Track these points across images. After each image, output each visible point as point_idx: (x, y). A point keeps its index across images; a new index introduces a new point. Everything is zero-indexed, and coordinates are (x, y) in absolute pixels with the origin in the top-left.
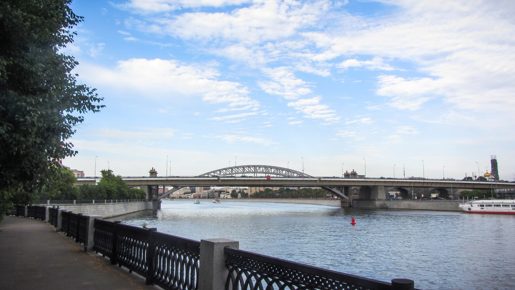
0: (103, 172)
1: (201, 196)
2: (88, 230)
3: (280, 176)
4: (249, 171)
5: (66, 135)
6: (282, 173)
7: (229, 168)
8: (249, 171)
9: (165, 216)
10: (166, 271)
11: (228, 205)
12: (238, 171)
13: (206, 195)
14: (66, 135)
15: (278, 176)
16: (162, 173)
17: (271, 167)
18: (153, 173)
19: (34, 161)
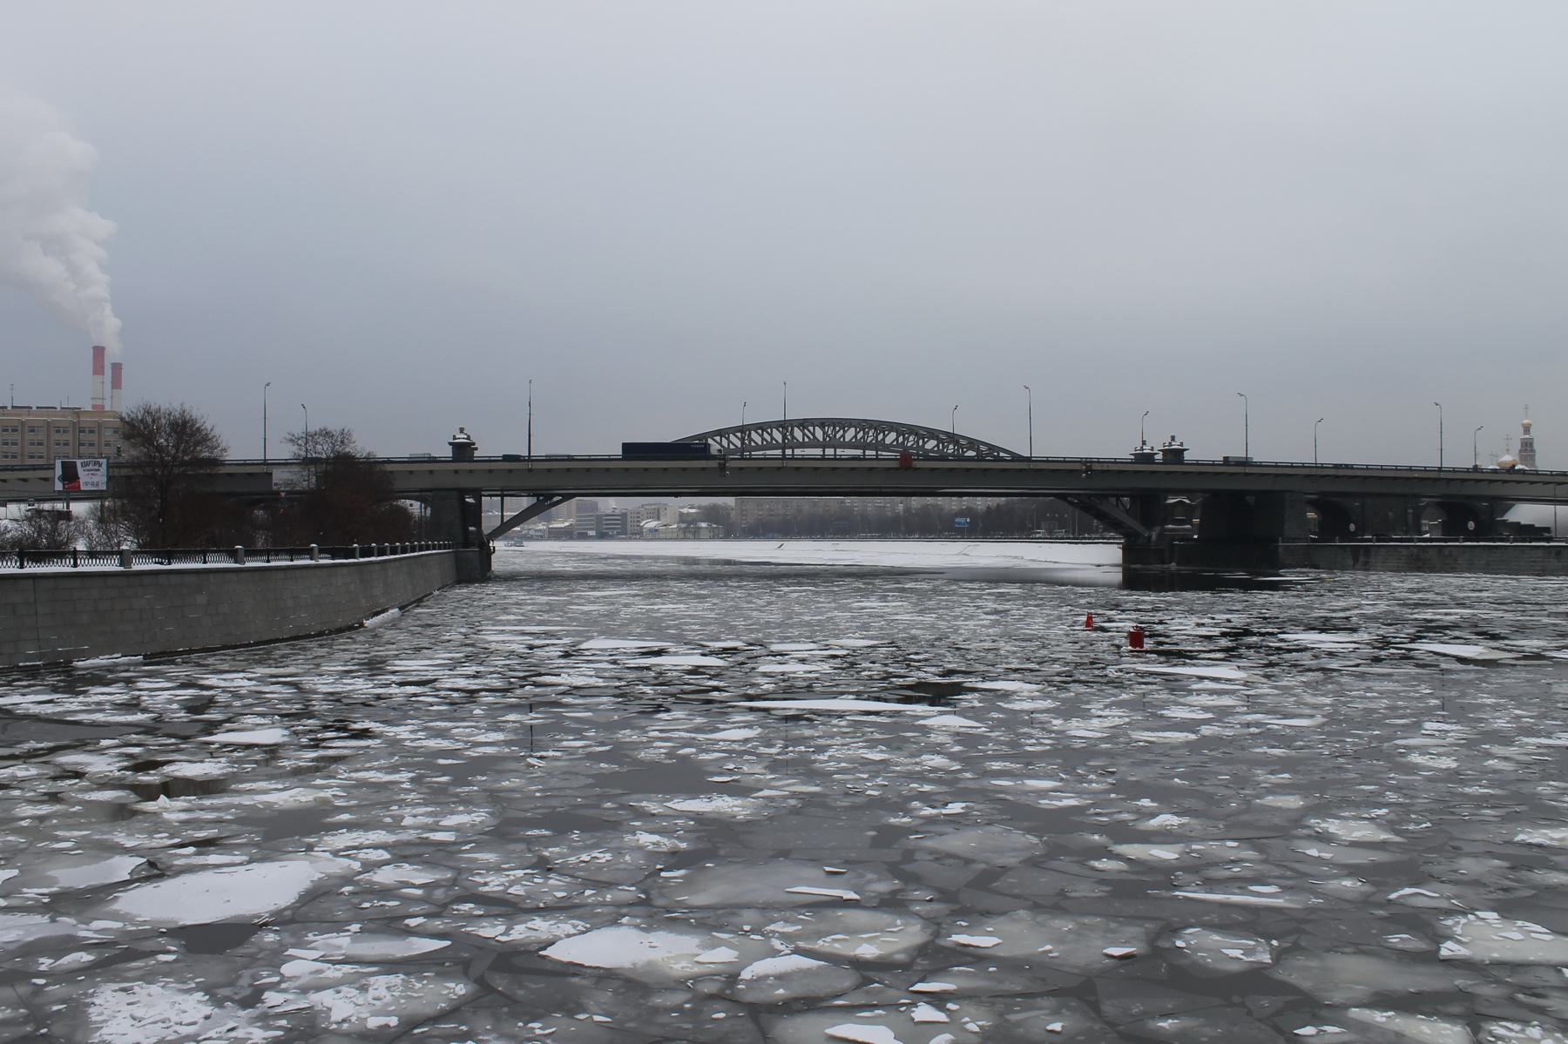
0: (1224, 458)
1: (576, 533)
2: (91, 886)
3: (877, 455)
4: (728, 439)
5: (439, 923)
6: (842, 439)
7: (734, 430)
8: (728, 439)
9: (761, 680)
10: (450, 761)
11: (1439, 614)
12: (838, 436)
13: (592, 525)
14: (439, 923)
15: (867, 452)
16: (489, 447)
17: (844, 424)
18: (463, 450)
19: (139, 508)
